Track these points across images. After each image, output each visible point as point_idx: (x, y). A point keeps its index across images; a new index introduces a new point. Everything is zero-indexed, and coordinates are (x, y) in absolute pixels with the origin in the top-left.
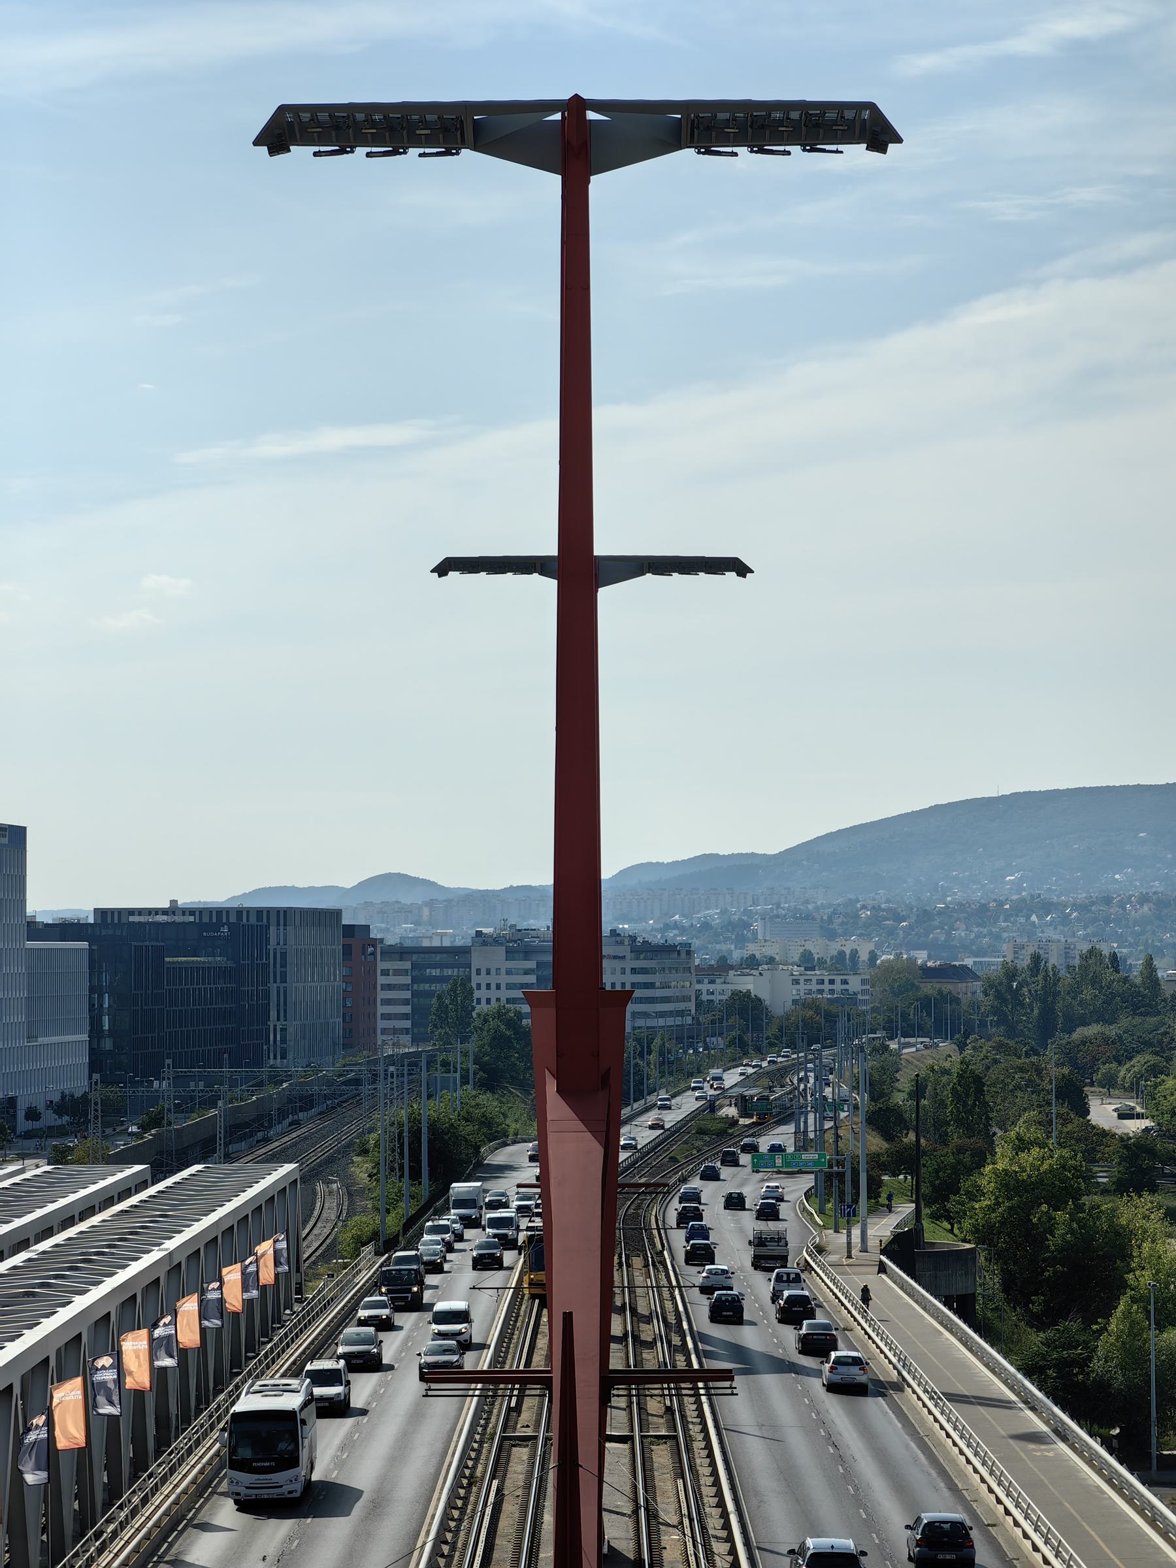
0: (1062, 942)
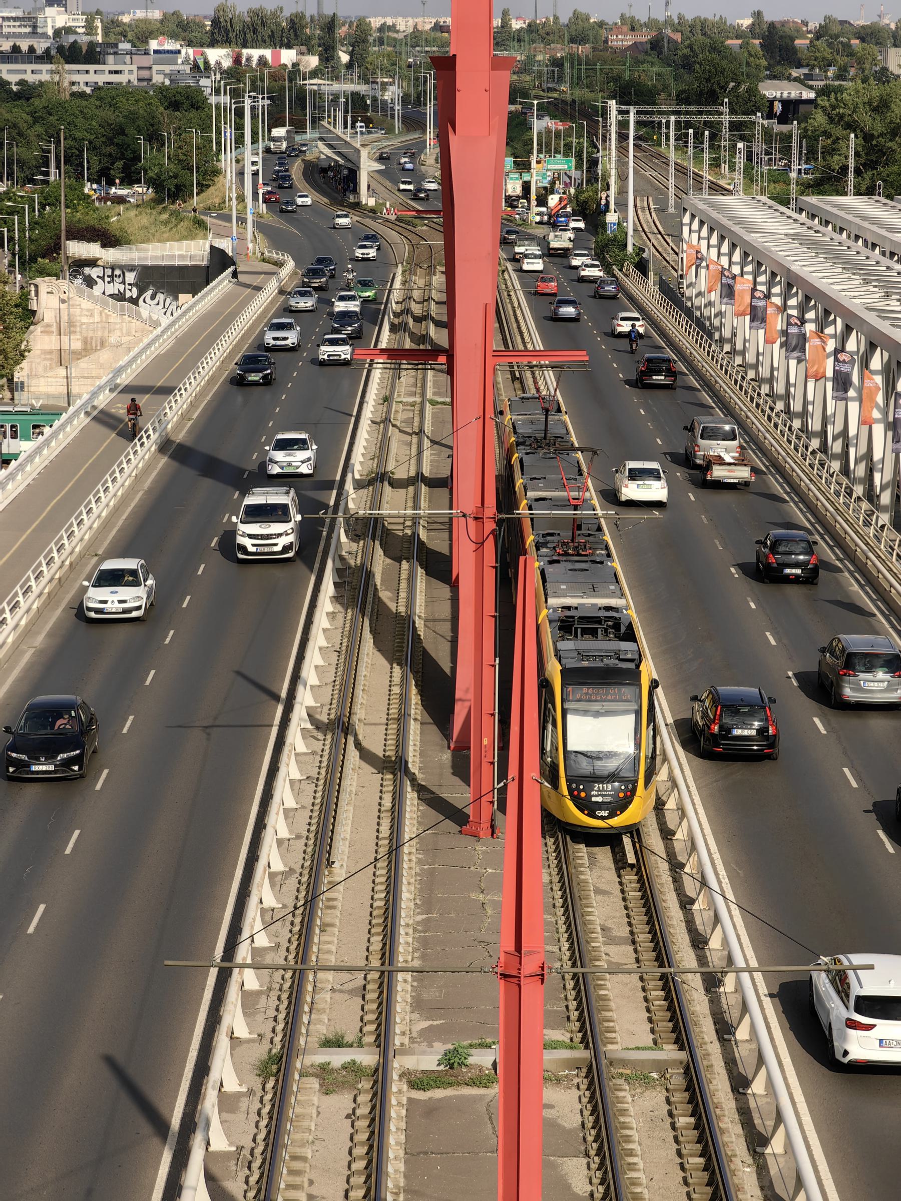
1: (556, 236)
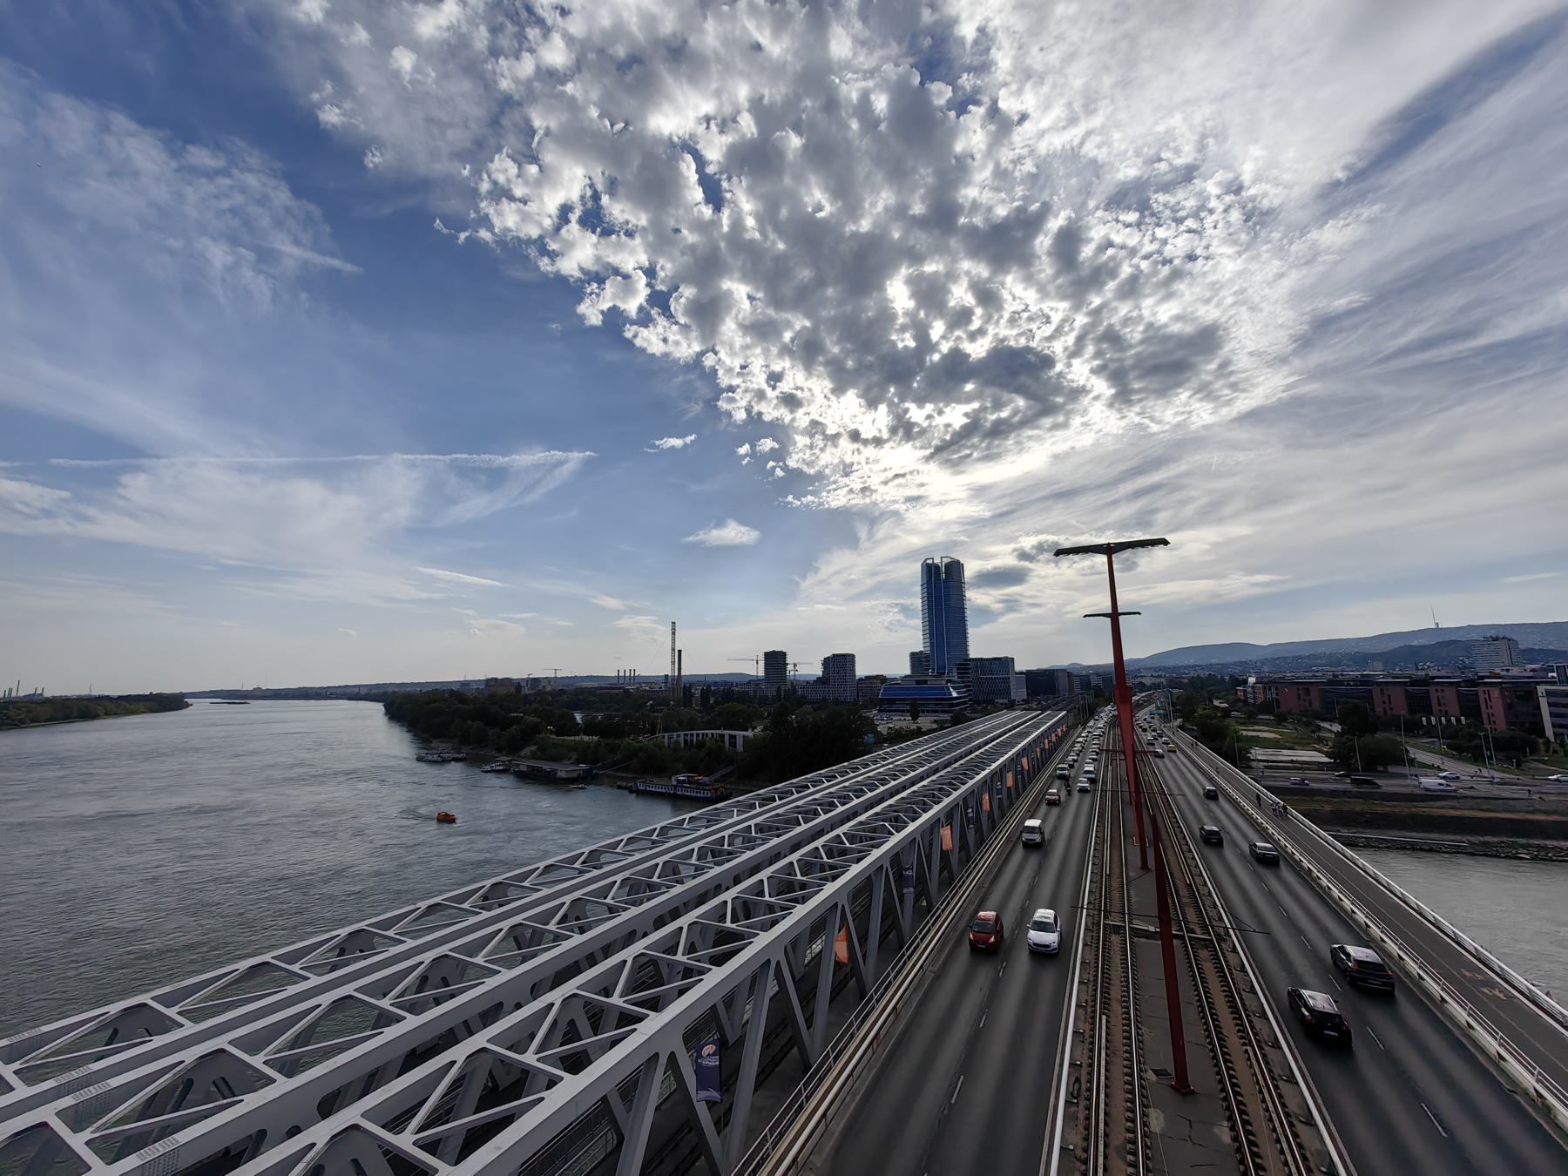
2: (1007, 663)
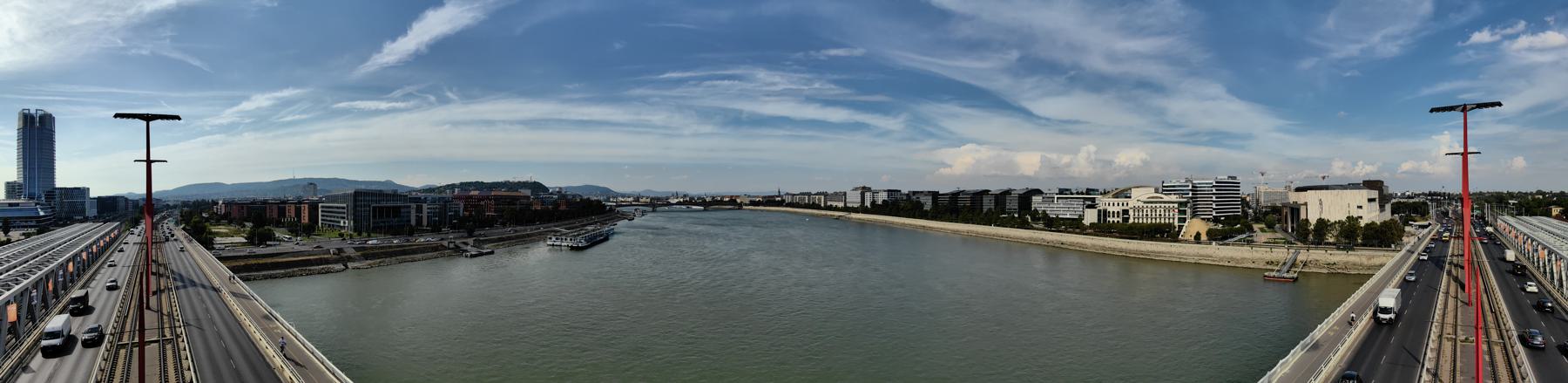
0: (261, 198)
1: (1123, 194)
2: (82, 192)
